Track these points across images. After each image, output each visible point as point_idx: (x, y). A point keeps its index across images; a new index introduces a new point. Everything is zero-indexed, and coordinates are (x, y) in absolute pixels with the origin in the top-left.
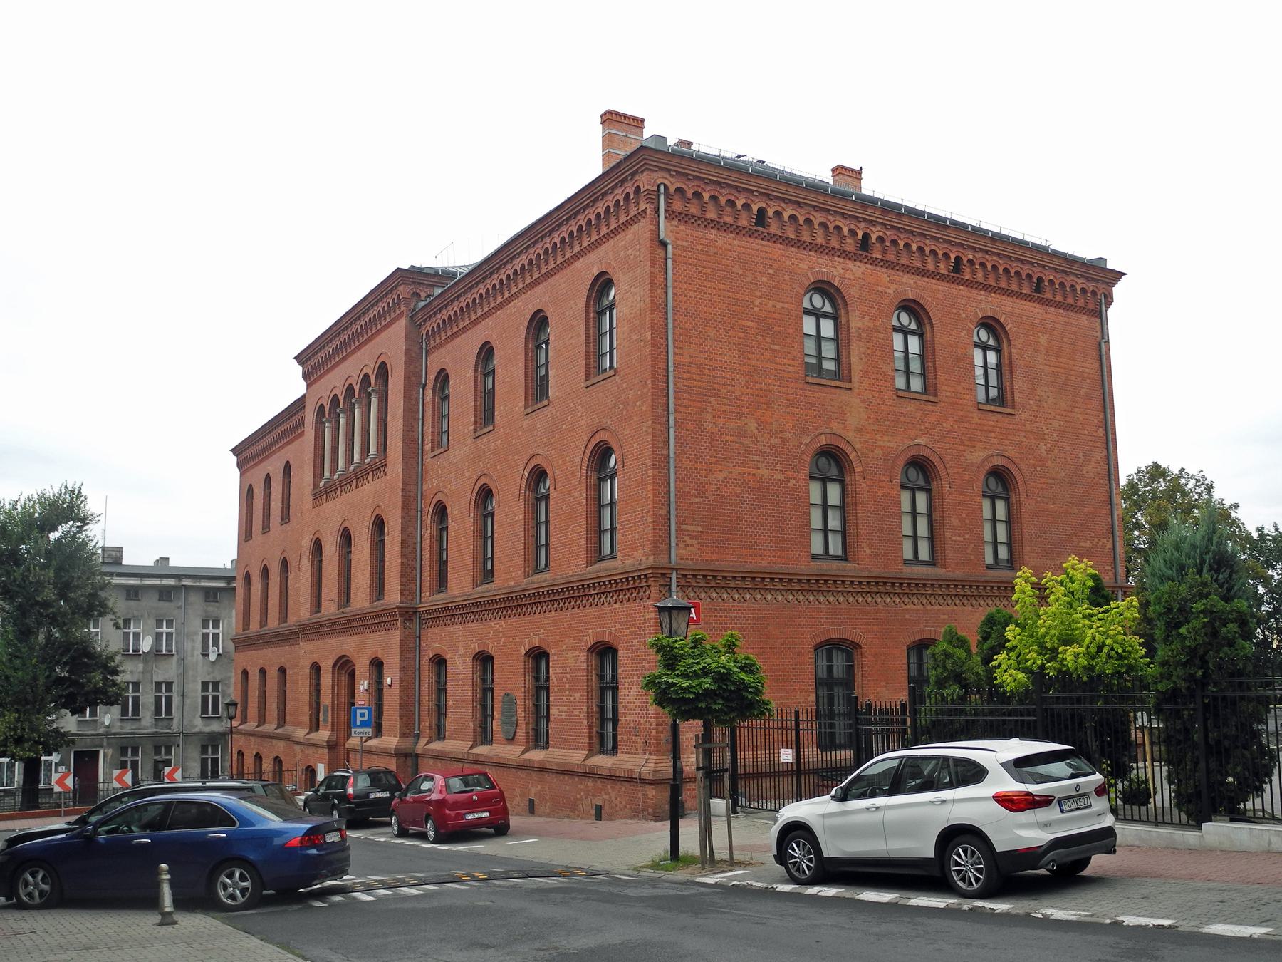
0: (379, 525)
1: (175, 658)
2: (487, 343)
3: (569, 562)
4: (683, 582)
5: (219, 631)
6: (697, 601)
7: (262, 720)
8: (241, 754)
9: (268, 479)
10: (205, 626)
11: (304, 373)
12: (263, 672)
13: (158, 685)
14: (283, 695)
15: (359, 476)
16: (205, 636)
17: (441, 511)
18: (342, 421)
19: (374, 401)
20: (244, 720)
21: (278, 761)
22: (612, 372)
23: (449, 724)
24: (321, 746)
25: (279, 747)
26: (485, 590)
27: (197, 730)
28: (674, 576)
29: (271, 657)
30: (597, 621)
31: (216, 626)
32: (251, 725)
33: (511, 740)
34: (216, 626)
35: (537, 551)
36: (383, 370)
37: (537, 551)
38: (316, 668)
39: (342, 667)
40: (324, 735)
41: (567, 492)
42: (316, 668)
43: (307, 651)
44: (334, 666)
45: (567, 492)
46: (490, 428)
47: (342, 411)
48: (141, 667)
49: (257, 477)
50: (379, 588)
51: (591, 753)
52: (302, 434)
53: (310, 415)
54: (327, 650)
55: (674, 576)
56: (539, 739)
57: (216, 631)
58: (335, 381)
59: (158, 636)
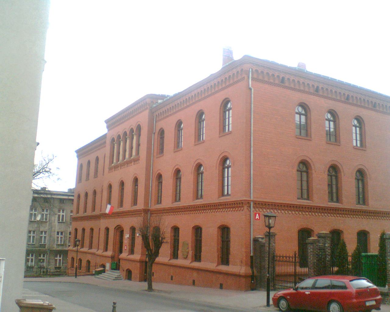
0: (136, 180)
1: (48, 223)
2: (180, 120)
3: (187, 199)
4: (254, 206)
5: (64, 214)
6: (259, 212)
7: (91, 247)
8: (73, 258)
9: (89, 162)
10: (59, 211)
11: (107, 126)
12: (84, 230)
13: (42, 232)
14: (92, 237)
15: (129, 163)
16: (59, 216)
17: (160, 176)
18: (122, 144)
19: (135, 138)
20: (82, 246)
21: (89, 262)
22: (181, 149)
23: (136, 250)
24: (109, 257)
25: (89, 257)
26: (176, 204)
27: (54, 249)
28: (252, 203)
29: (87, 225)
30: (199, 219)
31: (63, 211)
32: (85, 249)
33: (186, 258)
34: (63, 211)
35: (177, 197)
36: (139, 128)
37: (177, 197)
38: (107, 229)
39: (118, 229)
40: (109, 253)
41: (188, 178)
42: (107, 229)
43: (103, 223)
44: (115, 228)
45: (188, 178)
46: (161, 155)
47: (115, 143)
48: (36, 226)
49: (85, 161)
50: (135, 202)
51: (218, 265)
52: (105, 146)
53: (108, 142)
54: (112, 224)
55: (252, 203)
56: (197, 257)
57: (63, 214)
58: (120, 130)
59: (43, 215)
